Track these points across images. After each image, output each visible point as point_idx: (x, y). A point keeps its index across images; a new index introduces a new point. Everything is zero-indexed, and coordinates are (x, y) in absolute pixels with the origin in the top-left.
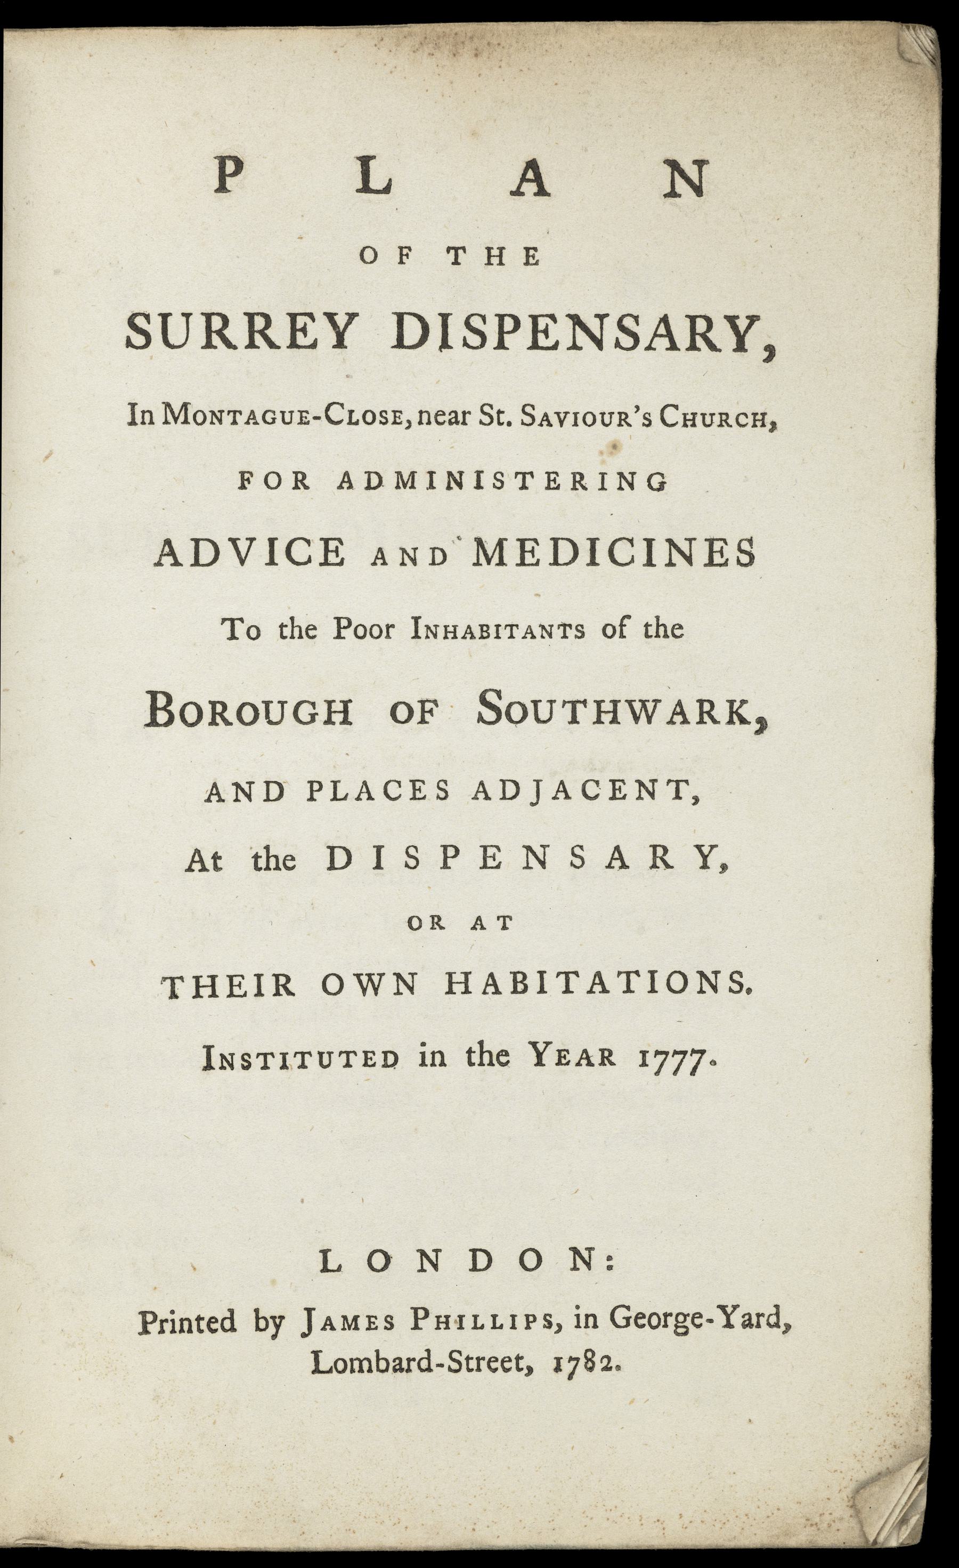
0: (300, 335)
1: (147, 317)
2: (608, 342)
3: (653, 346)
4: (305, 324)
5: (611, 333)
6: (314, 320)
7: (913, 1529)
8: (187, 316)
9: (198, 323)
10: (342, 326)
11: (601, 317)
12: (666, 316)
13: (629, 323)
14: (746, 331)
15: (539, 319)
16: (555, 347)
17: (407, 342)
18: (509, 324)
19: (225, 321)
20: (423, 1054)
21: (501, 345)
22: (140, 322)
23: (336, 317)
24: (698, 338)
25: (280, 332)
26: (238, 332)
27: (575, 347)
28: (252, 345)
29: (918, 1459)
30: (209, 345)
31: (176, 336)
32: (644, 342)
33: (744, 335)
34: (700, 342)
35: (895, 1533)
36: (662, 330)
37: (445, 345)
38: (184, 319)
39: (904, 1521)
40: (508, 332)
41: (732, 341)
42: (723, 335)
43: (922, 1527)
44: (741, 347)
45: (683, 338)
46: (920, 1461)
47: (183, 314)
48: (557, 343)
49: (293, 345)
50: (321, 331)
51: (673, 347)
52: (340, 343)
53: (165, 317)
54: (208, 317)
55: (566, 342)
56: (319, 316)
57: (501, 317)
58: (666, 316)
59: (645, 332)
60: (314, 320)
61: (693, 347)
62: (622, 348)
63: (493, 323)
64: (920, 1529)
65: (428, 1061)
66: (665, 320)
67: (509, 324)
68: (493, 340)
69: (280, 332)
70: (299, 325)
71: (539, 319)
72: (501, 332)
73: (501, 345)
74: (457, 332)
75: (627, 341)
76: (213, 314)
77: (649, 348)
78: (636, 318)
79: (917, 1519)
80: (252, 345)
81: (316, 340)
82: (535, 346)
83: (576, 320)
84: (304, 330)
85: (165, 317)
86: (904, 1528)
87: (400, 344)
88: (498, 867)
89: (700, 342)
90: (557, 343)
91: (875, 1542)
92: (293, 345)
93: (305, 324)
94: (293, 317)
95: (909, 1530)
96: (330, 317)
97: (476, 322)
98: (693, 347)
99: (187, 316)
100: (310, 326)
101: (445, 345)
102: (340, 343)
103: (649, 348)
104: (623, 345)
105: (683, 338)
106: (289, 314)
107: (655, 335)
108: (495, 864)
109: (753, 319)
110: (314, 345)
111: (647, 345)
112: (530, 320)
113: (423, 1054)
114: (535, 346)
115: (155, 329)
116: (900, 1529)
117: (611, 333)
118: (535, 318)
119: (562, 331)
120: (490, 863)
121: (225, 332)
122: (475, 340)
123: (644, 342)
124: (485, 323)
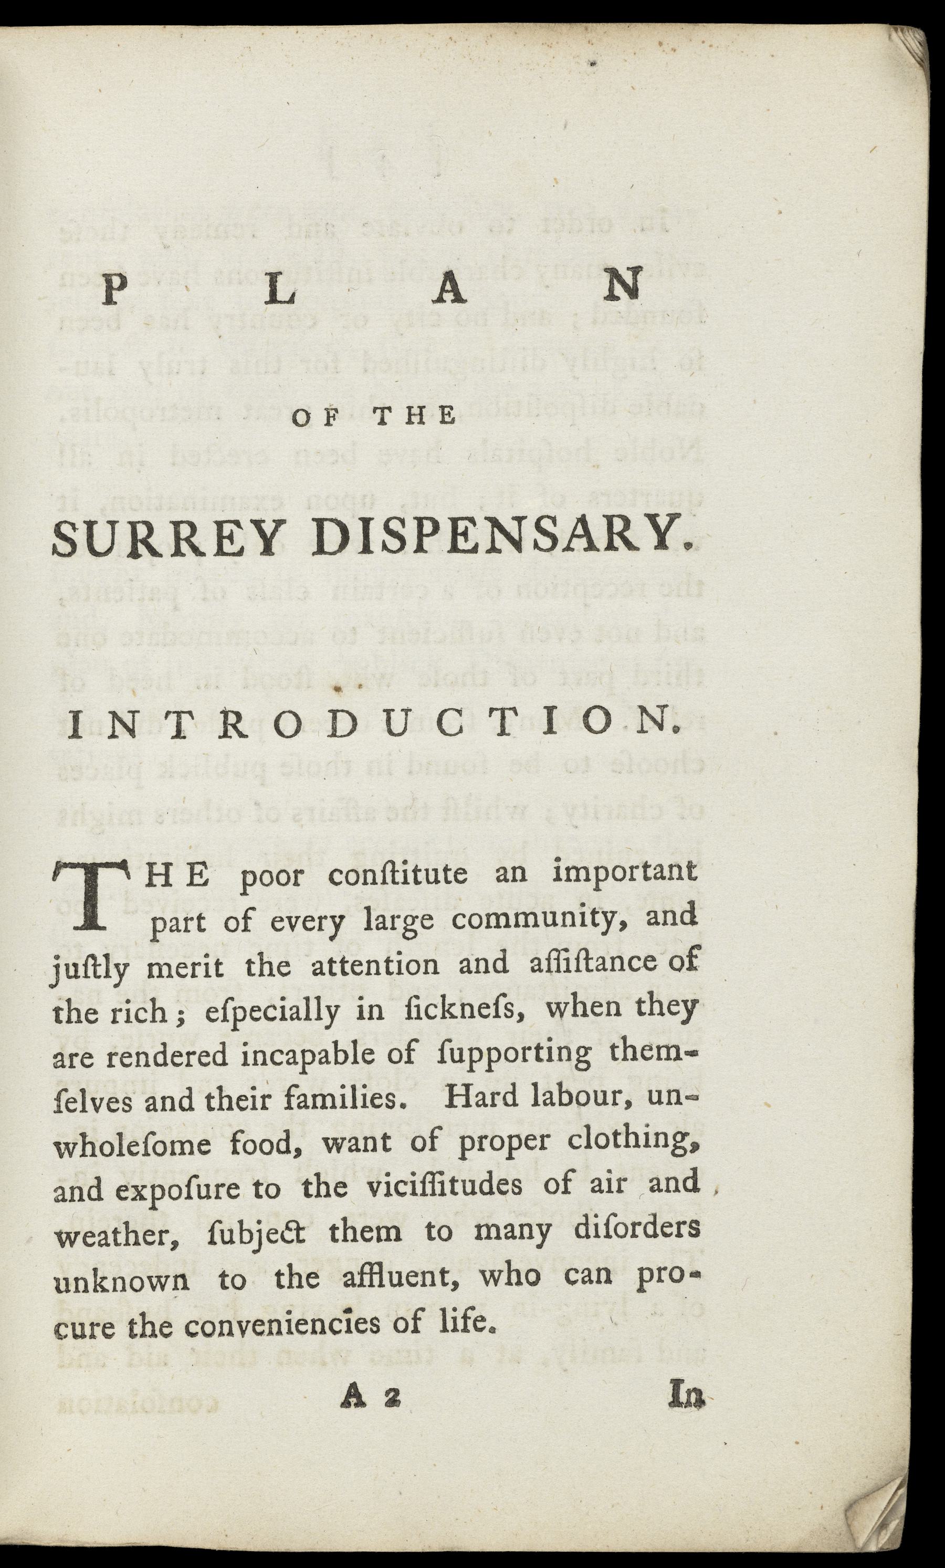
0: (226, 542)
1: (402, 522)
2: (527, 544)
3: (572, 546)
4: (466, 528)
5: (529, 533)
6: (475, 524)
7: (893, 1534)
8: (113, 523)
9: (123, 533)
10: (663, 528)
11: (519, 519)
12: (584, 516)
13: (546, 524)
14: (273, 534)
15: (224, 525)
16: (475, 550)
17: (327, 548)
18: (428, 527)
19: (627, 522)
20: (245, 1054)
21: (420, 548)
22: (66, 529)
23: (263, 525)
24: (616, 538)
25: (206, 539)
26: (163, 539)
27: (493, 549)
28: (178, 552)
29: (893, 1480)
30: (134, 554)
31: (101, 544)
32: (562, 543)
33: (665, 533)
34: (617, 541)
35: (875, 1537)
36: (580, 531)
37: (366, 549)
38: (109, 526)
39: (883, 1525)
40: (428, 535)
41: (654, 538)
42: (642, 533)
43: (901, 1532)
44: (662, 544)
45: (601, 539)
46: (898, 1482)
47: (109, 522)
48: (476, 545)
49: (220, 552)
50: (249, 538)
51: (591, 547)
52: (268, 550)
53: (90, 525)
54: (133, 525)
55: (485, 545)
56: (246, 523)
57: (420, 521)
58: (584, 516)
59: (563, 531)
60: (475, 524)
61: (611, 547)
62: (541, 549)
63: (412, 525)
64: (900, 1533)
65: (250, 1060)
66: (582, 520)
67: (428, 527)
68: (412, 543)
69: (206, 539)
70: (226, 533)
71: (224, 525)
72: (421, 535)
73: (420, 548)
74: (377, 534)
75: (545, 542)
76: (182, 522)
77: (568, 548)
78: (554, 520)
79: (896, 1524)
80: (178, 552)
81: (242, 549)
82: (454, 549)
83: (495, 523)
84: (231, 537)
85: (90, 525)
86: (884, 1532)
87: (320, 550)
88: (206, 883)
89: (617, 541)
90: (476, 545)
91: (862, 1548)
92: (220, 552)
93: (466, 528)
94: (220, 525)
95: (889, 1535)
96: (257, 524)
97: (395, 525)
98: (611, 547)
99: (113, 523)
100: (472, 530)
101: (366, 549)
102: (268, 550)
103: (568, 548)
104: (389, 547)
105: (601, 539)
106: (216, 522)
107: (573, 535)
108: (202, 881)
109: (673, 517)
110: (240, 552)
111: (565, 546)
112: (450, 523)
113: (245, 1054)
114: (454, 549)
115: (80, 537)
116: (880, 1533)
117: (529, 533)
118: (455, 521)
119: (481, 534)
120: (197, 879)
121: (192, 539)
122: (394, 544)
123: (562, 543)
124: (555, 525)
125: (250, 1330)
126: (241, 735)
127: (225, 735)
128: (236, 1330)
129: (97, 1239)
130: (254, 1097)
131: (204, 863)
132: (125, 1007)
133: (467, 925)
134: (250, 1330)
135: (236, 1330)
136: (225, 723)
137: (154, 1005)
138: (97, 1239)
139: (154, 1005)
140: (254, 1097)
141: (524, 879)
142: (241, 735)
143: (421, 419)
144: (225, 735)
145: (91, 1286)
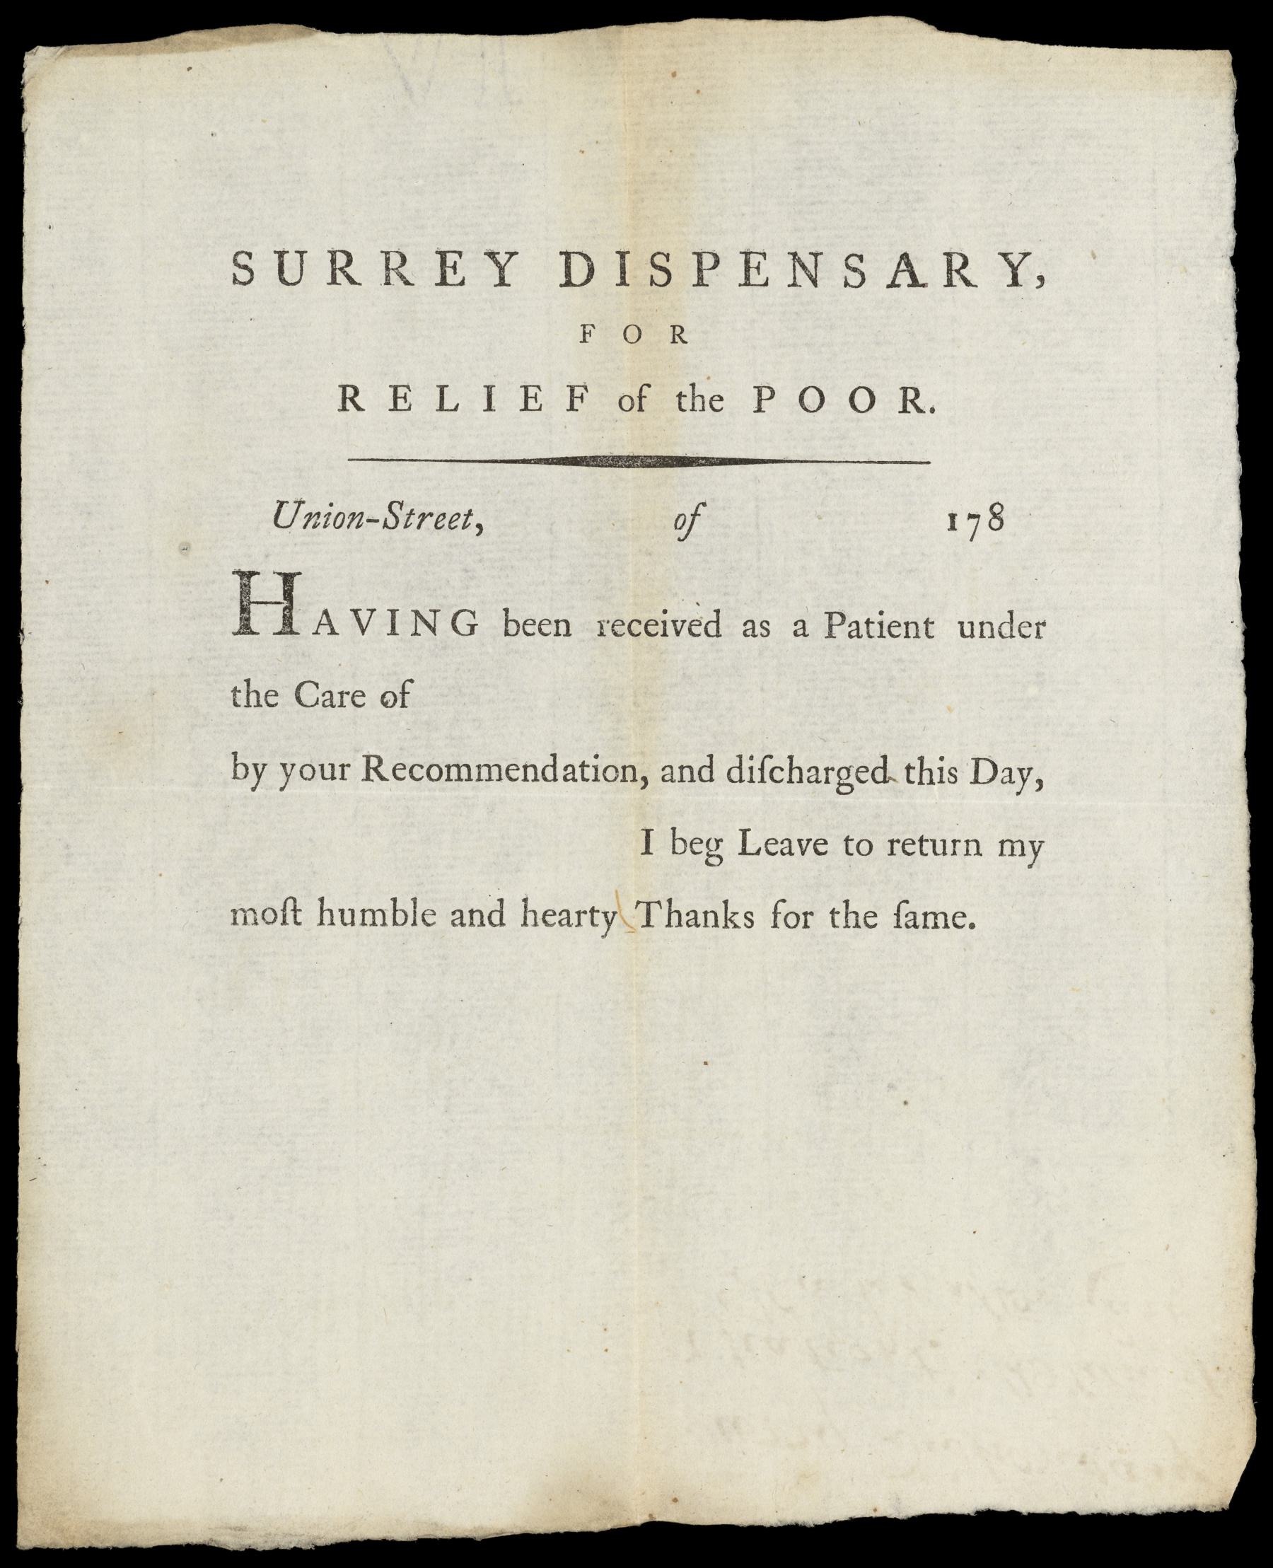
36: (324, 621)
120: (755, 278)
125: (685, 631)
126: (359, 408)
127: (905, 410)
128: (670, 630)
129: (779, 847)
130: (664, 623)
131: (460, 254)
132: (593, 762)
133: (537, 632)
134: (685, 631)
135: (670, 630)
136: (949, 270)
137: (847, 907)
138: (779, 847)
139: (847, 907)
140: (664, 623)
141: (568, 634)
142: (359, 408)
143: (245, 590)
144: (905, 410)
145: (721, 922)
